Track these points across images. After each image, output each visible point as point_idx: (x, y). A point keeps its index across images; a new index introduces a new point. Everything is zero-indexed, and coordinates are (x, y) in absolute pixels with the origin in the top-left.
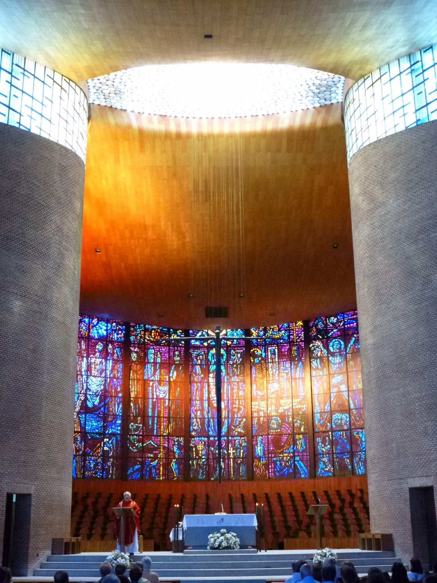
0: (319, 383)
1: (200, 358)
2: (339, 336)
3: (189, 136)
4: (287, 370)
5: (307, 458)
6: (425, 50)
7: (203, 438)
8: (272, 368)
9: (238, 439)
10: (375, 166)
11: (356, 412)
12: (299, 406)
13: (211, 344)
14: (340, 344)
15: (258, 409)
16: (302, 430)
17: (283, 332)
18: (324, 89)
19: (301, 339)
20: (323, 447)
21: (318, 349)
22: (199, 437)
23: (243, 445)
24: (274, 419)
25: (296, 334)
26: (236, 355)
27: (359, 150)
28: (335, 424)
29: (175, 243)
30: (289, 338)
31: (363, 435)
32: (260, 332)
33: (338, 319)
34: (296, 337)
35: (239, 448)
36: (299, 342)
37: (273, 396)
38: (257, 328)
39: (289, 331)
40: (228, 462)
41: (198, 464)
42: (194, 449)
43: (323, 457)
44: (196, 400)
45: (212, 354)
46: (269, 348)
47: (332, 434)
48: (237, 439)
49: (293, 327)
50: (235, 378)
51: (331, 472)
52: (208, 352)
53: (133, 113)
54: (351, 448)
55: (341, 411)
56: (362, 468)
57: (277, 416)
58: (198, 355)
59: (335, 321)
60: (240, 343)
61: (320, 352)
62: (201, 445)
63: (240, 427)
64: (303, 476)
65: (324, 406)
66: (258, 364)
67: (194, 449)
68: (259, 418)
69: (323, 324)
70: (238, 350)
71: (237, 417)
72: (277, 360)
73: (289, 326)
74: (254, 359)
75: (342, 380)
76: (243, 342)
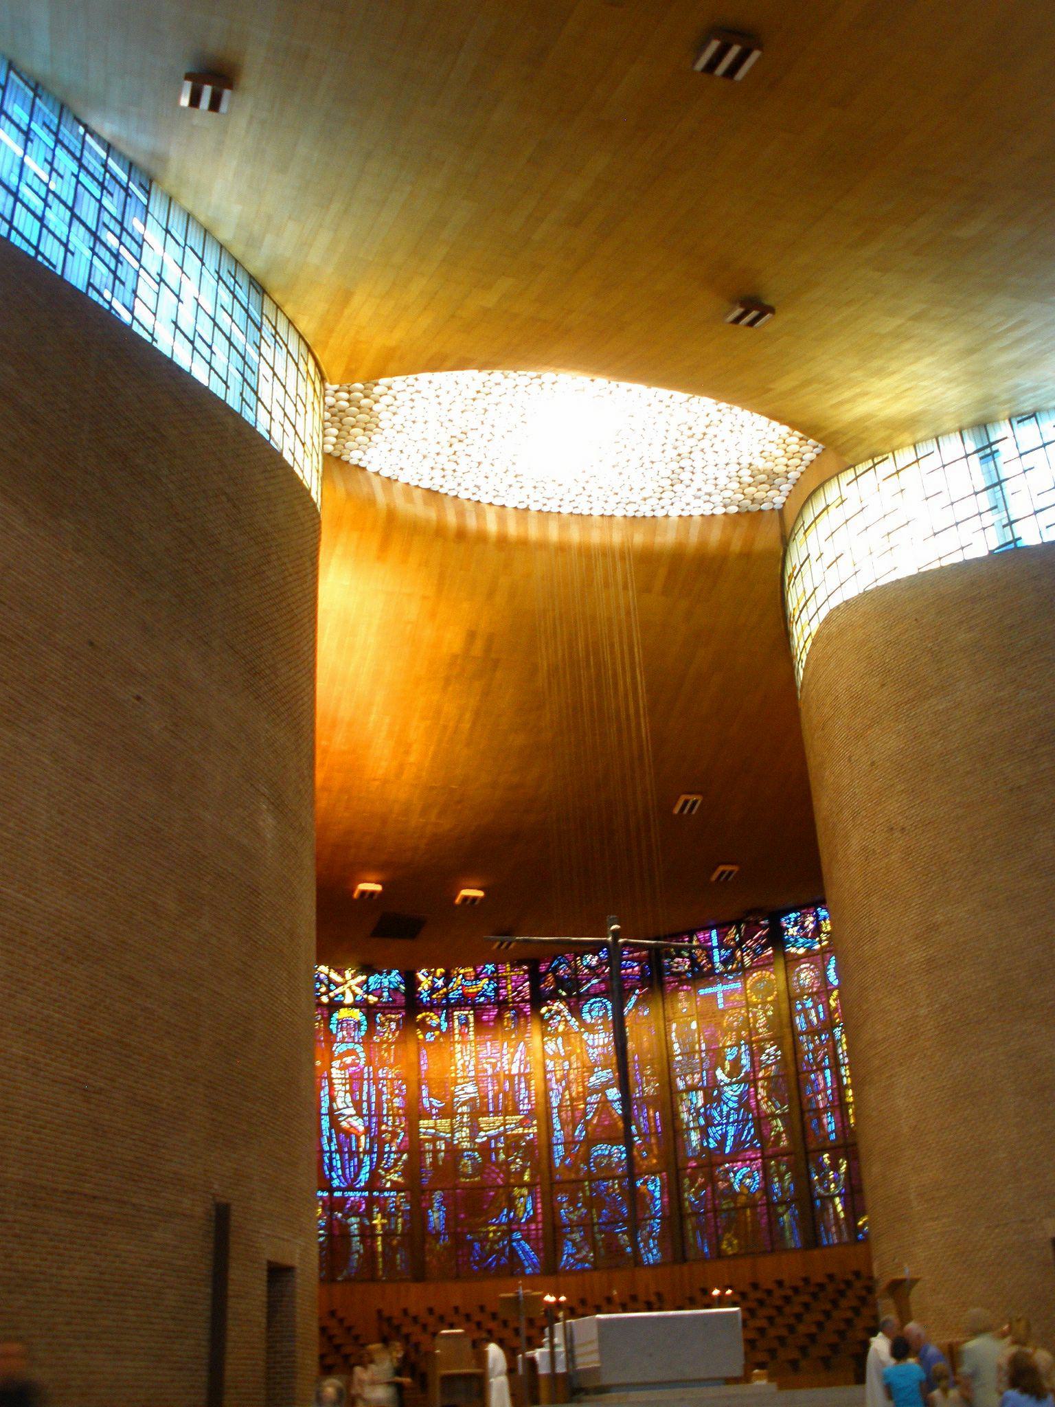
0: (561, 1085)
4: (493, 1058)
6: (1019, 419)
8: (462, 1052)
10: (916, 620)
11: (640, 1142)
12: (520, 1130)
13: (336, 999)
14: (606, 1008)
15: (433, 1135)
16: (526, 1178)
17: (486, 981)
18: (763, 477)
19: (523, 997)
20: (571, 1212)
21: (559, 1018)
23: (402, 1208)
24: (468, 1156)
25: (512, 987)
27: (865, 592)
28: (597, 1165)
29: (384, 764)
32: (436, 980)
33: (600, 958)
34: (513, 992)
35: (393, 1214)
36: (519, 1002)
37: (465, 1109)
39: (498, 980)
43: (572, 1232)
45: (338, 1020)
46: (456, 1013)
47: (590, 1186)
50: (385, 1071)
52: (331, 1016)
55: (610, 1139)
56: (655, 1251)
57: (473, 1150)
60: (394, 1001)
63: (396, 1172)
64: (529, 1270)
68: (436, 1152)
69: (570, 967)
70: (391, 1014)
71: (390, 1152)
72: (472, 1037)
73: (497, 969)
74: (424, 1035)
75: (610, 1080)
76: (401, 1000)
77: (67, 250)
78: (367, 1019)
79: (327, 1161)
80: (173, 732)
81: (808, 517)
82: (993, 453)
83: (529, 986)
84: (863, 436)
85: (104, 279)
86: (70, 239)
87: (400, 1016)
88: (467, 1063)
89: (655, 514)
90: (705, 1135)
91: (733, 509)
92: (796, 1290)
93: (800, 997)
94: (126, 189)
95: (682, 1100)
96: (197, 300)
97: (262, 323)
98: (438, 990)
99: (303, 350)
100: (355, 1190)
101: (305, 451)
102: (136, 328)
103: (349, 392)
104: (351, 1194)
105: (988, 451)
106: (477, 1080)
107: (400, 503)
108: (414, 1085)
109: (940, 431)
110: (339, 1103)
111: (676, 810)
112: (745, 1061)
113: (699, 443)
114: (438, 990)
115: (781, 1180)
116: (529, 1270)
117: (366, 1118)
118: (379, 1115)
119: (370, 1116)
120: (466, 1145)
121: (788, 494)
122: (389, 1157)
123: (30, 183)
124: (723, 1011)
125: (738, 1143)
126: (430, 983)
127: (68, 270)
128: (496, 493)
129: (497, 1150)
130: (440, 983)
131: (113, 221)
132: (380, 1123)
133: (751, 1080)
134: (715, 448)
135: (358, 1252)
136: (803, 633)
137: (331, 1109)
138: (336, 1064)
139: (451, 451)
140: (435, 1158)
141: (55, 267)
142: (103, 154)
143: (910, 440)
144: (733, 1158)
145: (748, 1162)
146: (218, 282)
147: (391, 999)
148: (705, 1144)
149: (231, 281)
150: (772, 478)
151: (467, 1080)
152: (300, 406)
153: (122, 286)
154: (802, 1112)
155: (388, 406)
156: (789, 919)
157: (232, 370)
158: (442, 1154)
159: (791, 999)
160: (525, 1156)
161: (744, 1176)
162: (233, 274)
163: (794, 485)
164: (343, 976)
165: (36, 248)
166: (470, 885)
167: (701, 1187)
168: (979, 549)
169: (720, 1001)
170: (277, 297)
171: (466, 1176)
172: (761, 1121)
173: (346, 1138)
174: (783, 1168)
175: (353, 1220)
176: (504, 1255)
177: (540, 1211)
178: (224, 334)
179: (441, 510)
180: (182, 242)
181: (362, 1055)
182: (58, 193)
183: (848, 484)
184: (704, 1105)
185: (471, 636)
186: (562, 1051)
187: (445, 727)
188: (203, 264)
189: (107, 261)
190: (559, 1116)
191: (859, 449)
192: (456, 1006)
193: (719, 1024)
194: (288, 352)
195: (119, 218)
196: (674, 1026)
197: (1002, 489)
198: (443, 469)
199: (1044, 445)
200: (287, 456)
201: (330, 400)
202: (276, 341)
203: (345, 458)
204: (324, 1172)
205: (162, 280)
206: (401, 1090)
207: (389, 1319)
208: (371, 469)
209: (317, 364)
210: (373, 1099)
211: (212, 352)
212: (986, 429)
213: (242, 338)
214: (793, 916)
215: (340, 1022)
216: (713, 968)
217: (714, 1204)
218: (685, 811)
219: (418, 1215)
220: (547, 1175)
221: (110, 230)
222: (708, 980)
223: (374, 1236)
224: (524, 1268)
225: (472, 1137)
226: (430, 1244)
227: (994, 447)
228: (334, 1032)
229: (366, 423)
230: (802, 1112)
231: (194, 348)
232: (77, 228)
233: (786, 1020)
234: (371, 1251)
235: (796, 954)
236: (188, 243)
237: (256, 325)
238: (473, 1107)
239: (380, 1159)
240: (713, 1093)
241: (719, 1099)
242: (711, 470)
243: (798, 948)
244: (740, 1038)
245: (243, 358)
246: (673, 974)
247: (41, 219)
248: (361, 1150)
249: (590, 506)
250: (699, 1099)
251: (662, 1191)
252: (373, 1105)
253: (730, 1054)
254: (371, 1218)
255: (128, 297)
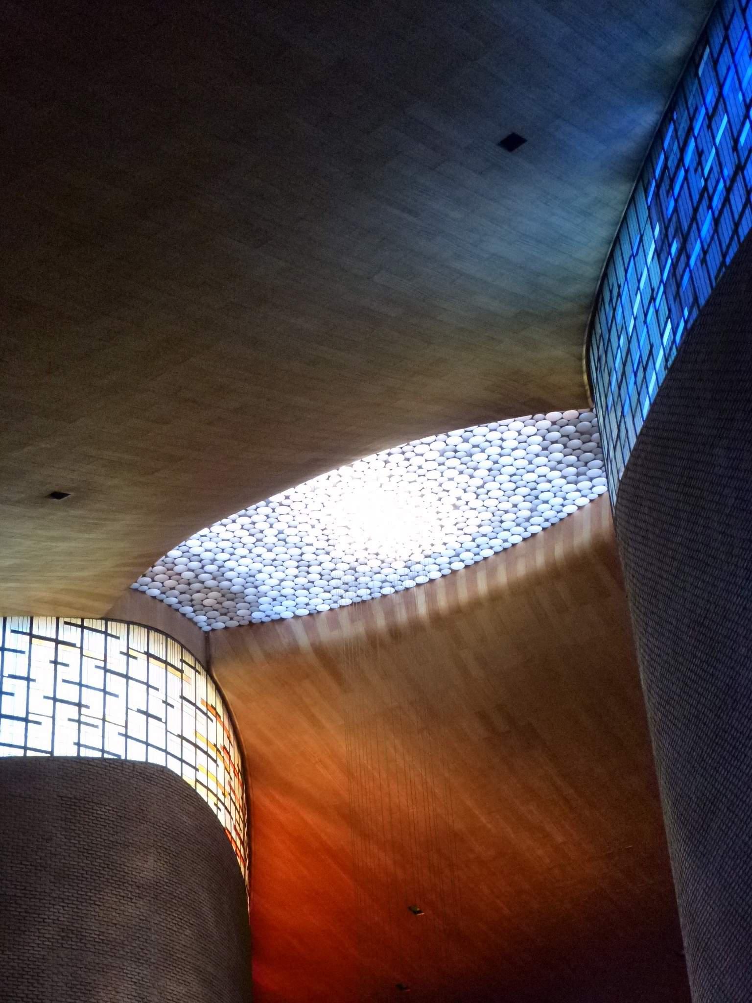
3: (416, 626)
53: (300, 621)
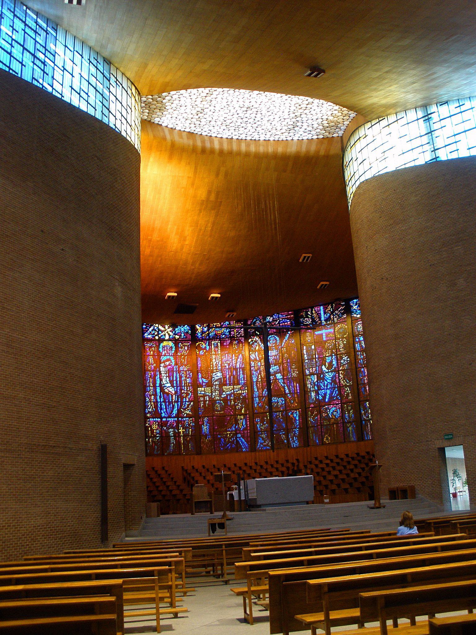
0: (257, 372)
1: (152, 350)
2: (275, 333)
4: (229, 361)
5: (247, 435)
6: (441, 104)
7: (157, 419)
8: (215, 359)
9: (187, 420)
14: (276, 339)
15: (204, 394)
16: (243, 411)
18: (333, 124)
20: (261, 426)
21: (256, 344)
22: (153, 418)
25: (236, 331)
26: (183, 347)
27: (374, 177)
29: (175, 245)
30: (230, 334)
31: (297, 415)
32: (204, 328)
33: (273, 318)
35: (188, 427)
37: (217, 383)
38: (202, 324)
40: (179, 439)
41: (152, 441)
42: (149, 428)
44: (150, 386)
45: (163, 346)
46: (212, 342)
48: (186, 420)
49: (234, 324)
50: (183, 367)
51: (269, 446)
52: (159, 345)
54: (287, 425)
57: (220, 400)
58: (151, 347)
59: (271, 320)
60: (186, 337)
61: (258, 346)
62: (156, 425)
63: (188, 410)
64: (244, 450)
65: (263, 392)
66: (203, 355)
67: (149, 428)
68: (205, 401)
71: (186, 401)
72: (220, 353)
73: (230, 323)
74: (199, 352)
76: (189, 337)
77: (22, 65)
78: (175, 346)
79: (159, 406)
80: (77, 261)
81: (352, 142)
82: (429, 119)
83: (244, 330)
84: (374, 110)
85: (39, 75)
86: (23, 59)
87: (189, 344)
88: (217, 363)
89: (287, 139)
90: (317, 393)
91: (321, 137)
92: (353, 458)
93: (358, 335)
94: (46, 31)
95: (308, 379)
96: (80, 74)
97: (110, 77)
98: (205, 332)
99: (129, 83)
100: (171, 417)
101: (131, 129)
102: (55, 93)
103: (152, 96)
104: (170, 419)
105: (427, 118)
106: (222, 371)
107: (176, 138)
108: (196, 373)
109: (406, 108)
110: (164, 381)
111: (301, 261)
112: (334, 362)
113: (304, 111)
114: (205, 332)
115: (349, 413)
116: (244, 450)
117: (175, 388)
118: (181, 386)
119: (177, 387)
120: (217, 398)
121: (352, 118)
122: (185, 403)
123: (4, 38)
124: (326, 341)
125: (331, 397)
126: (201, 329)
127: (23, 74)
128: (218, 133)
129: (230, 400)
130: (206, 329)
131: (41, 47)
132: (181, 390)
133: (337, 371)
134: (311, 113)
135: (173, 443)
136: (351, 190)
137: (160, 384)
138: (162, 365)
139: (197, 117)
140: (204, 403)
141: (17, 74)
142: (35, 17)
143: (394, 112)
144: (329, 403)
145: (335, 405)
146: (89, 64)
147: (185, 337)
148: (317, 397)
149: (95, 62)
150: (337, 126)
151: (218, 370)
152: (129, 110)
153: (47, 76)
154: (358, 385)
155: (169, 100)
156: (354, 302)
157: (97, 101)
158: (208, 402)
159: (354, 336)
160: (242, 402)
161: (333, 411)
162: (96, 59)
163: (347, 127)
164: (165, 328)
165: (9, 67)
166: (215, 292)
167: (316, 415)
168: (421, 162)
169: (324, 337)
170: (116, 65)
171: (218, 411)
172: (341, 388)
173: (167, 396)
174: (350, 408)
175: (171, 430)
176: (234, 444)
177: (248, 425)
178: (93, 86)
179: (195, 140)
180: (72, 50)
181: (173, 361)
182: (17, 40)
183: (368, 129)
184: (317, 381)
185: (209, 192)
186: (257, 358)
187: (200, 229)
188: (82, 57)
189: (40, 66)
190: (257, 385)
191: (372, 115)
192: (213, 339)
193: (324, 347)
194: (123, 87)
195: (44, 45)
196: (305, 347)
197: (432, 135)
198: (195, 124)
199: (450, 116)
200: (124, 134)
201: (144, 99)
202: (117, 84)
203: (152, 121)
204: (158, 410)
205: (64, 69)
206: (190, 375)
207: (186, 471)
208: (164, 125)
209: (136, 88)
210: (178, 379)
211: (88, 96)
212: (426, 108)
213: (101, 86)
214: (355, 301)
215: (163, 347)
216: (321, 323)
217: (321, 423)
218: (305, 261)
219: (198, 427)
220: (251, 410)
221: (40, 51)
222: (319, 328)
223: (180, 437)
224: (242, 448)
225: (220, 395)
226: (203, 439)
227: (429, 116)
228: (161, 352)
229: (160, 107)
230: (358, 385)
231: (80, 96)
232: (26, 54)
233: (352, 346)
234: (178, 442)
235: (356, 317)
236: (75, 49)
237: (107, 79)
238: (220, 382)
239: (181, 406)
240: (320, 376)
241: (324, 379)
242: (310, 122)
243: (357, 315)
244: (332, 352)
245: (102, 95)
246: (304, 325)
247: (10, 54)
248: (173, 401)
249: (259, 136)
250: (315, 378)
251: (299, 417)
252: (178, 382)
253: (328, 360)
254: (178, 430)
255: (50, 79)
